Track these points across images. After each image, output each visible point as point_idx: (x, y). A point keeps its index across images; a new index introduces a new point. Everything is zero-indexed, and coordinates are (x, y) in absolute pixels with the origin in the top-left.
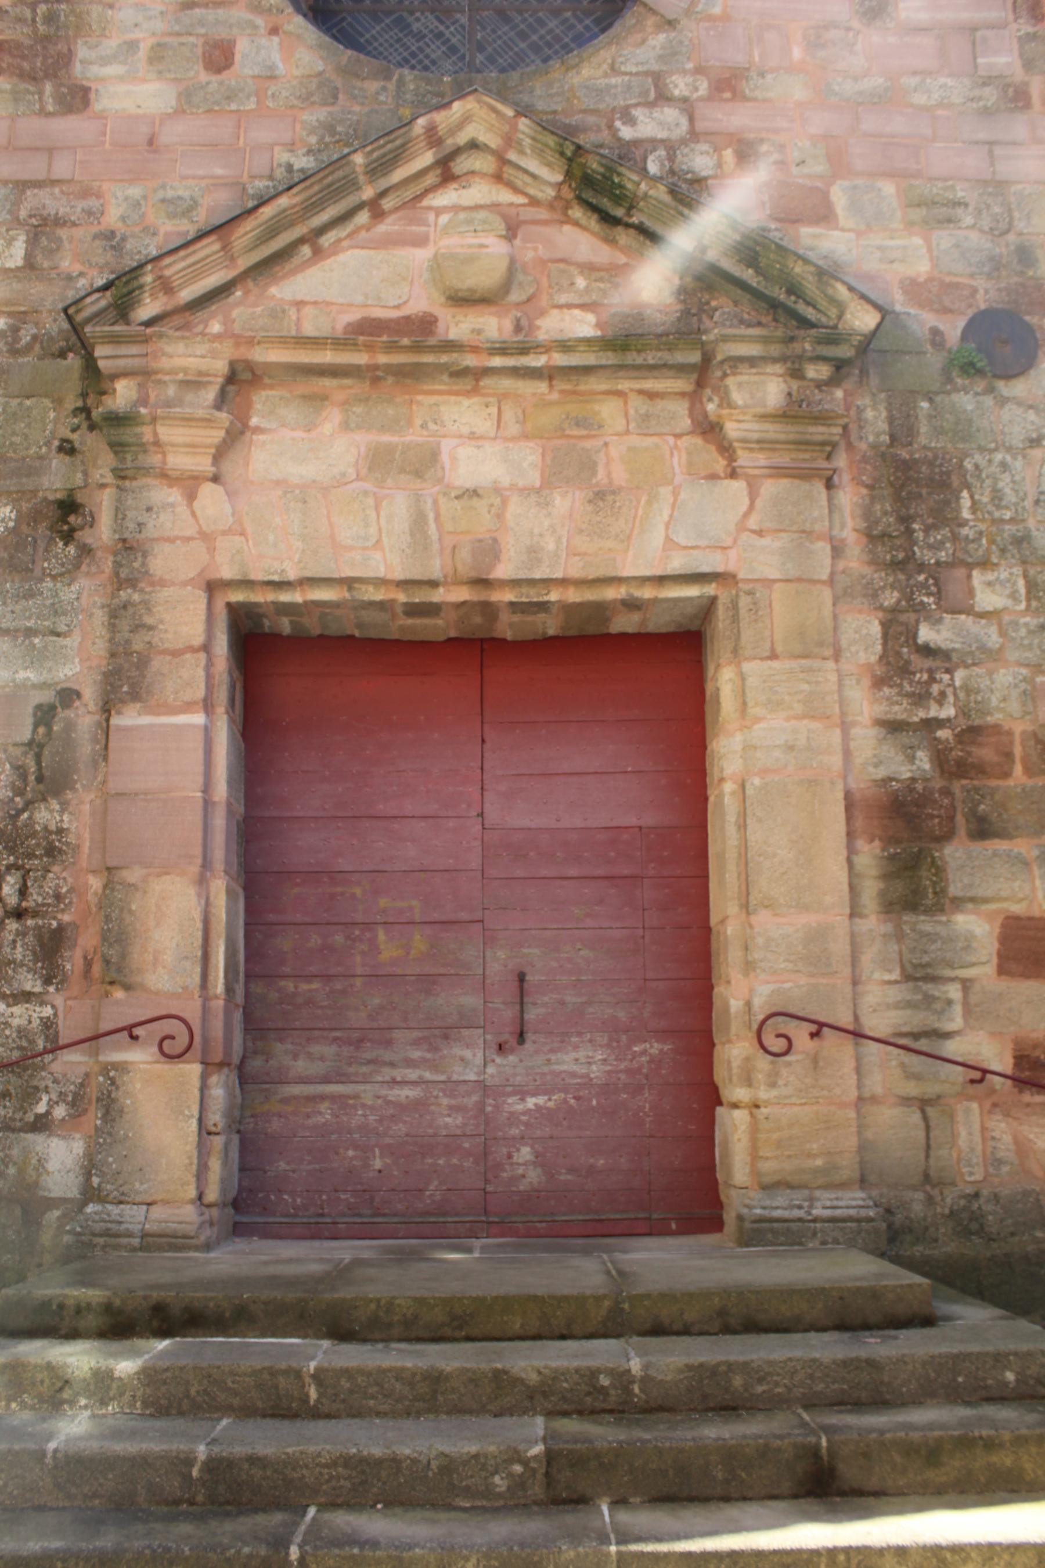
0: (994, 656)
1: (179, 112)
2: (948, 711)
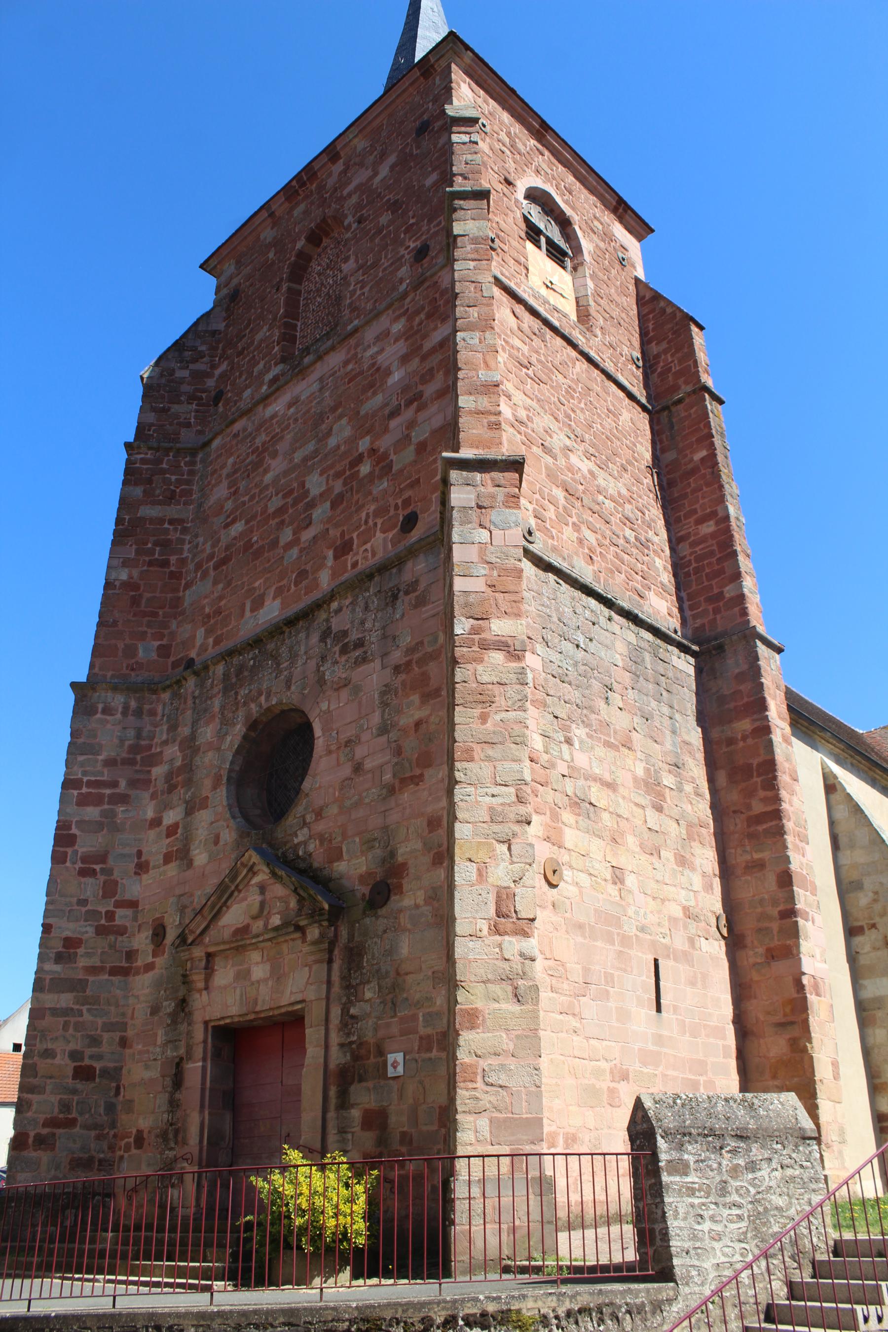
1: (209, 862)
2: (355, 1038)
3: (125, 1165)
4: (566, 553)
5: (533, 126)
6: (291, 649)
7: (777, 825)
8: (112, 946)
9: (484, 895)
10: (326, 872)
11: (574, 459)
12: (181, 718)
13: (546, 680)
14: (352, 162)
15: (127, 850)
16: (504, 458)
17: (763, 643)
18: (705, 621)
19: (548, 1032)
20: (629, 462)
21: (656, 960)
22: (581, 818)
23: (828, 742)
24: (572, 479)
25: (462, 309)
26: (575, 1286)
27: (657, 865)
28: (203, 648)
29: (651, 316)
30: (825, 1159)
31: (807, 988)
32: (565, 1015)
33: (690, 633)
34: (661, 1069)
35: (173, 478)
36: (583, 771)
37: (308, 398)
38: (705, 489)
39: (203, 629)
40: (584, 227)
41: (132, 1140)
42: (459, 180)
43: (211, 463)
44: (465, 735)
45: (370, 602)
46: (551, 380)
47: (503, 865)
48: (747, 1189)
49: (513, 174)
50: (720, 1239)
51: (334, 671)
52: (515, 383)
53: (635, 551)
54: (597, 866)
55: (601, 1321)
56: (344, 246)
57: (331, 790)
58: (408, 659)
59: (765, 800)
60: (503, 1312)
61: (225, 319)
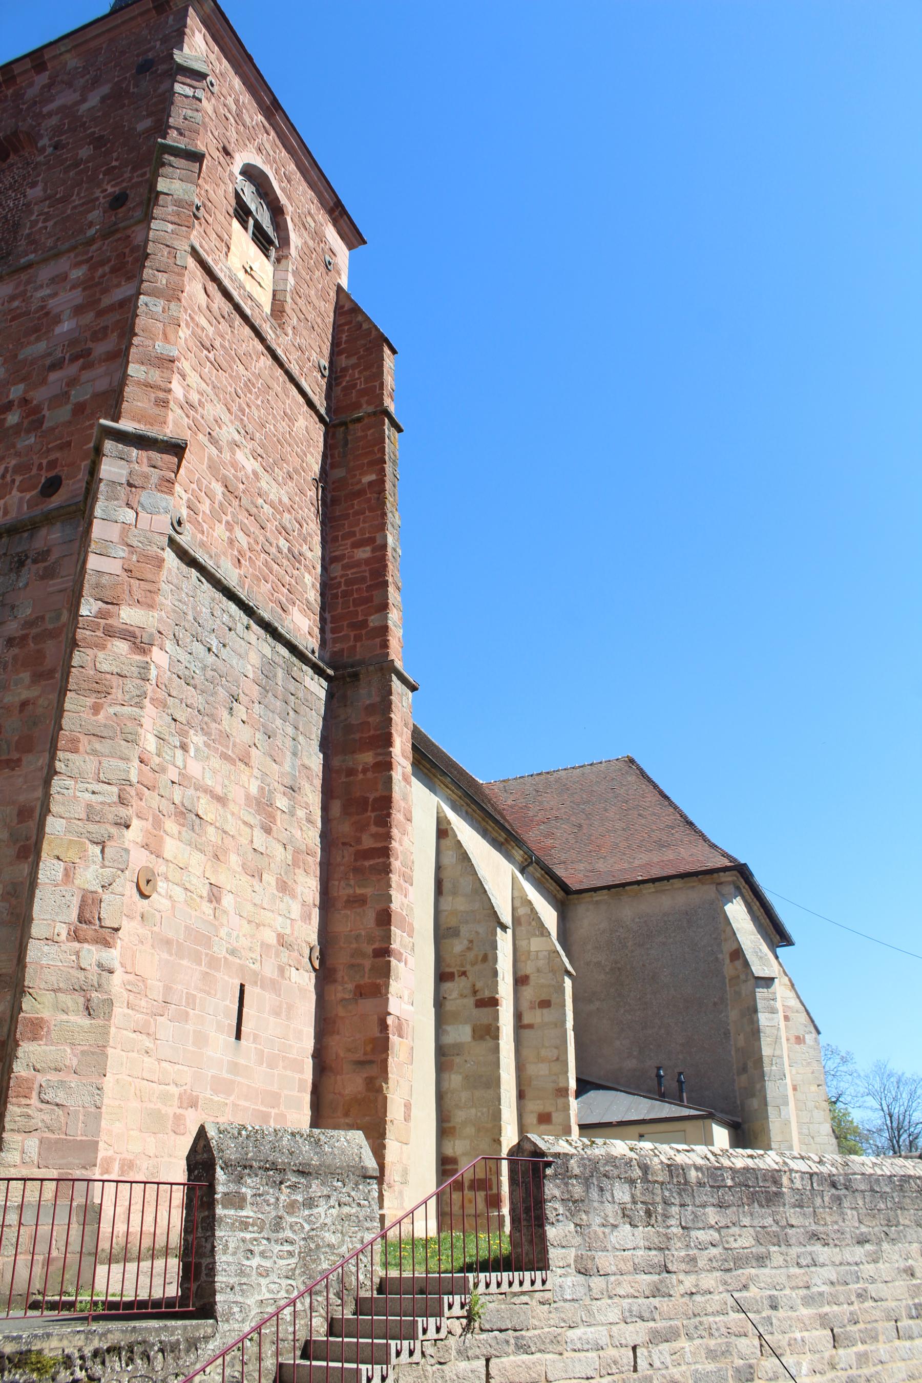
4: (214, 551)
5: (264, 101)
7: (384, 862)
9: (68, 898)
11: (240, 456)
13: (170, 679)
14: (59, 78)
16: (165, 438)
17: (399, 679)
18: (345, 646)
19: (118, 1051)
20: (296, 471)
21: (242, 986)
22: (185, 829)
23: (447, 787)
24: (233, 475)
25: (150, 271)
26: (108, 1323)
27: (257, 888)
29: (346, 328)
30: (386, 1199)
31: (390, 1029)
32: (138, 1033)
33: (327, 656)
34: (232, 1098)
36: (194, 780)
38: (367, 513)
40: (296, 220)
42: (174, 133)
44: (73, 724)
46: (231, 368)
47: (93, 867)
48: (302, 1226)
49: (233, 145)
50: (268, 1275)
52: (193, 363)
53: (285, 562)
54: (194, 880)
55: (131, 1360)
56: (34, 169)
58: (23, 632)
59: (375, 836)
60: (21, 1353)
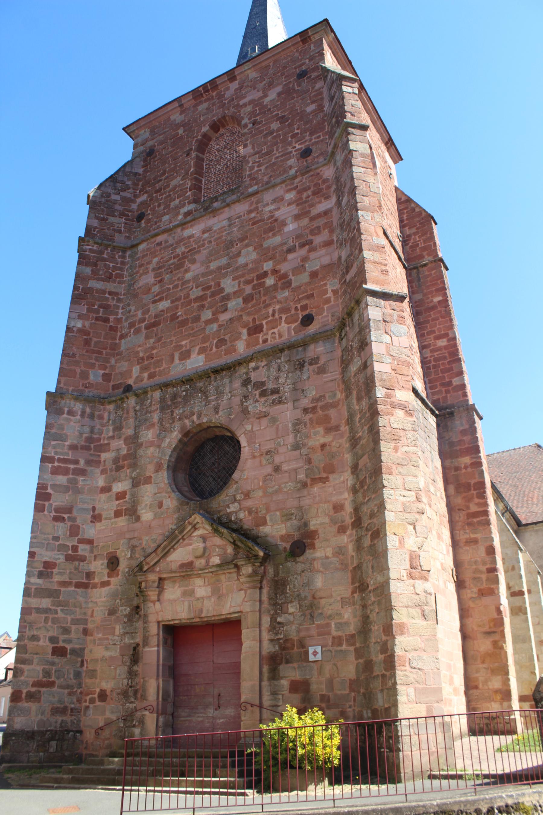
0: (292, 623)
1: (154, 519)
2: (282, 636)
3: (91, 712)
6: (217, 388)
7: (486, 519)
8: (76, 569)
9: (404, 555)
10: (254, 532)
12: (124, 423)
14: (245, 84)
15: (85, 506)
28: (139, 379)
29: (405, 211)
35: (111, 265)
37: (219, 229)
38: (440, 319)
39: (138, 367)
41: (96, 696)
42: (348, 115)
43: (139, 259)
45: (282, 366)
51: (256, 407)
57: (256, 481)
58: (313, 405)
59: (478, 504)
60: (515, 804)
61: (143, 167)
